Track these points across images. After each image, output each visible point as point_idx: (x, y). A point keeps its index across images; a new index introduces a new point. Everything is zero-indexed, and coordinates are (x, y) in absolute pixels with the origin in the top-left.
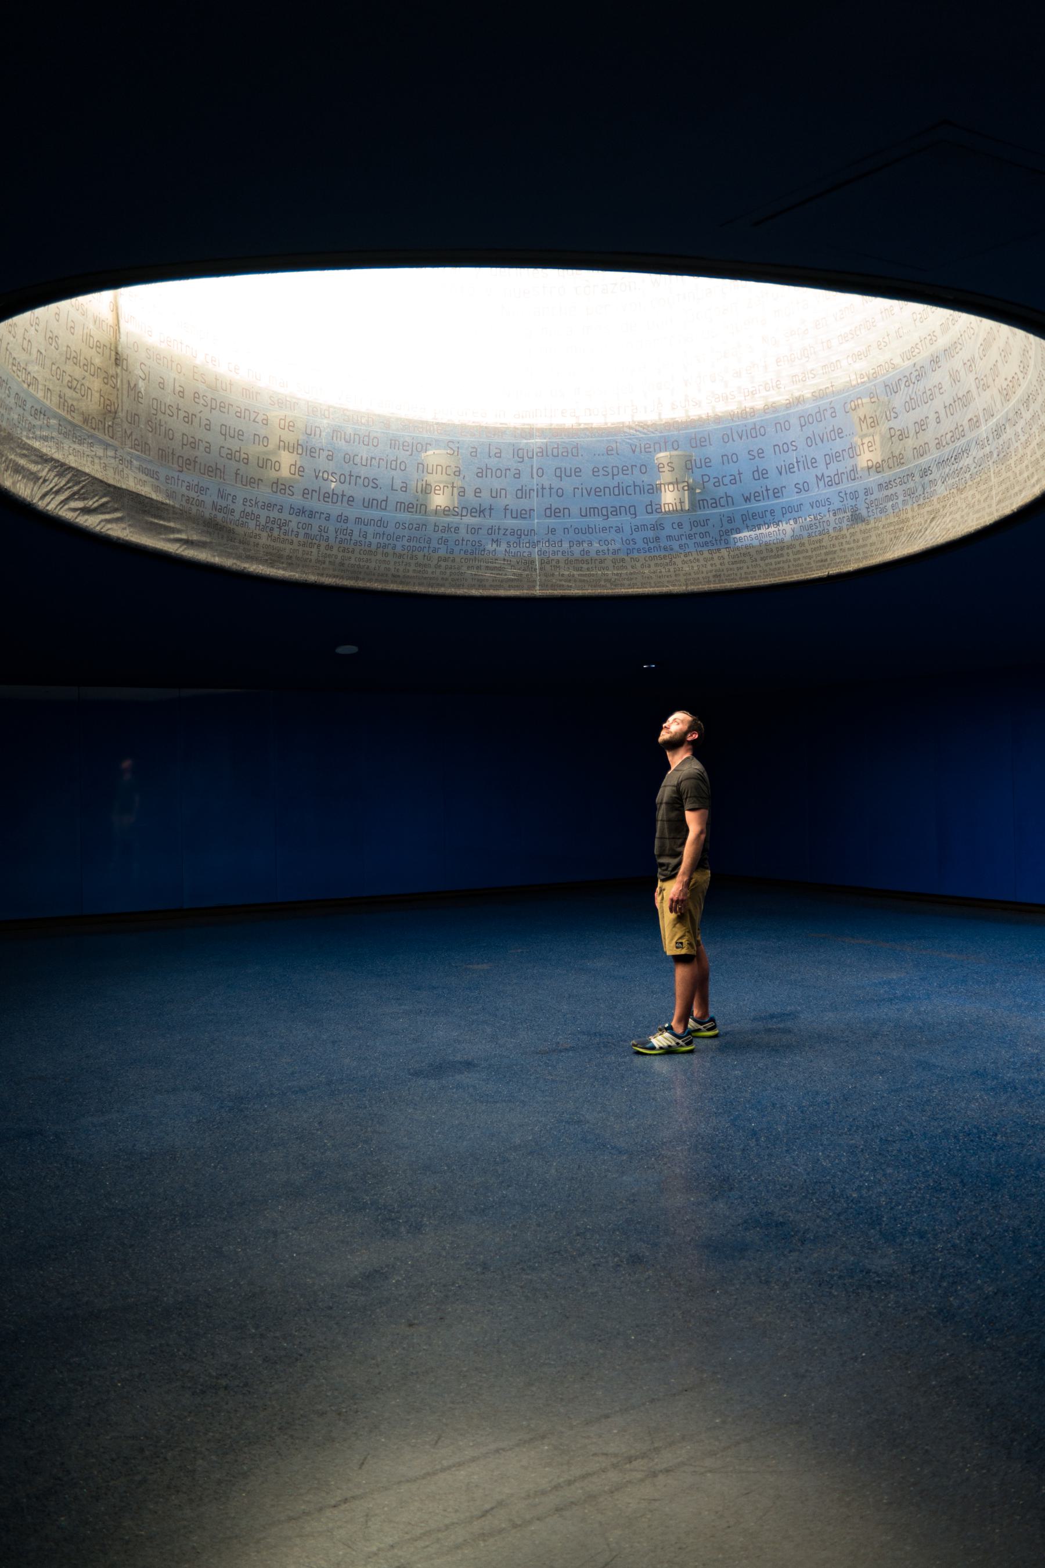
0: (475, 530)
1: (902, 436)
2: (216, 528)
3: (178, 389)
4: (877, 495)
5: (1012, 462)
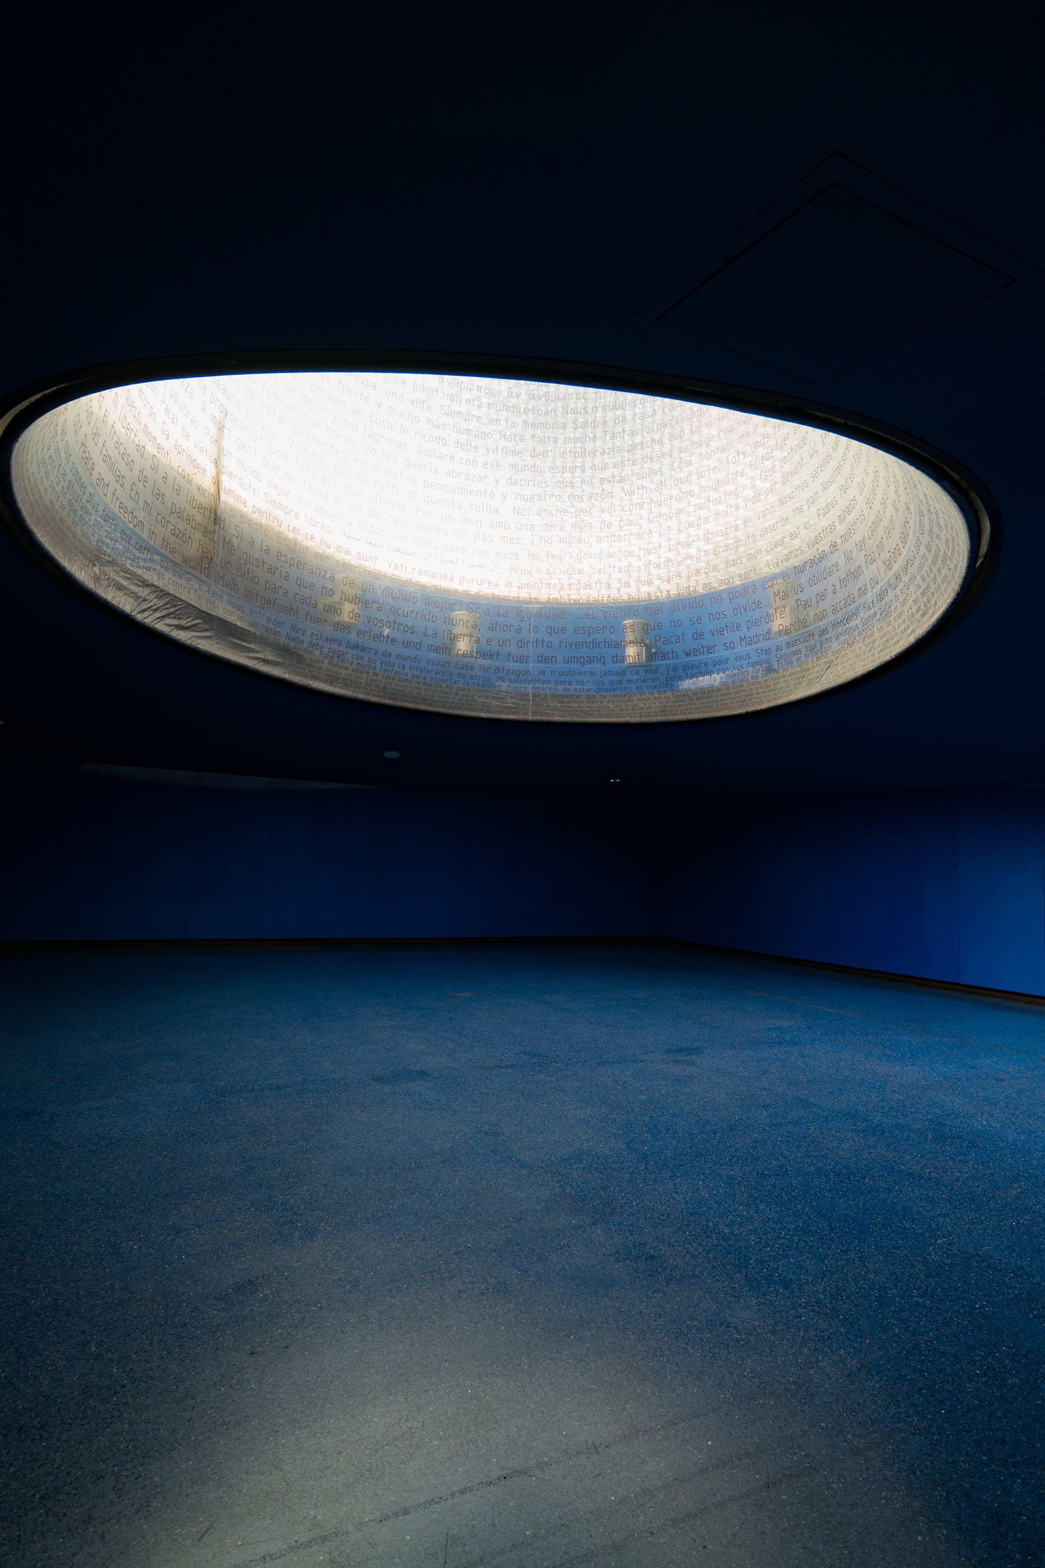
0: (485, 669)
1: (807, 605)
2: (288, 653)
3: (264, 547)
4: (785, 651)
5: (892, 618)
